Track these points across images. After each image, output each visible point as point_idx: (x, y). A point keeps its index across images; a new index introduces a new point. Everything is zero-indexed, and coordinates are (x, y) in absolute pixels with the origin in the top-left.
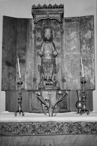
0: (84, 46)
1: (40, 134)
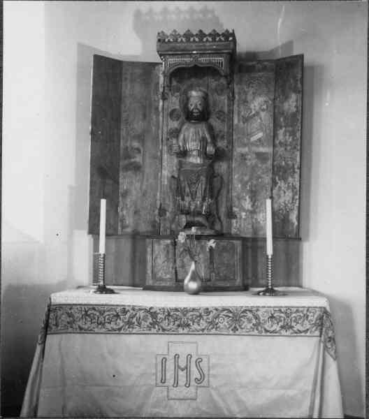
0: (281, 132)
1: (83, 331)
